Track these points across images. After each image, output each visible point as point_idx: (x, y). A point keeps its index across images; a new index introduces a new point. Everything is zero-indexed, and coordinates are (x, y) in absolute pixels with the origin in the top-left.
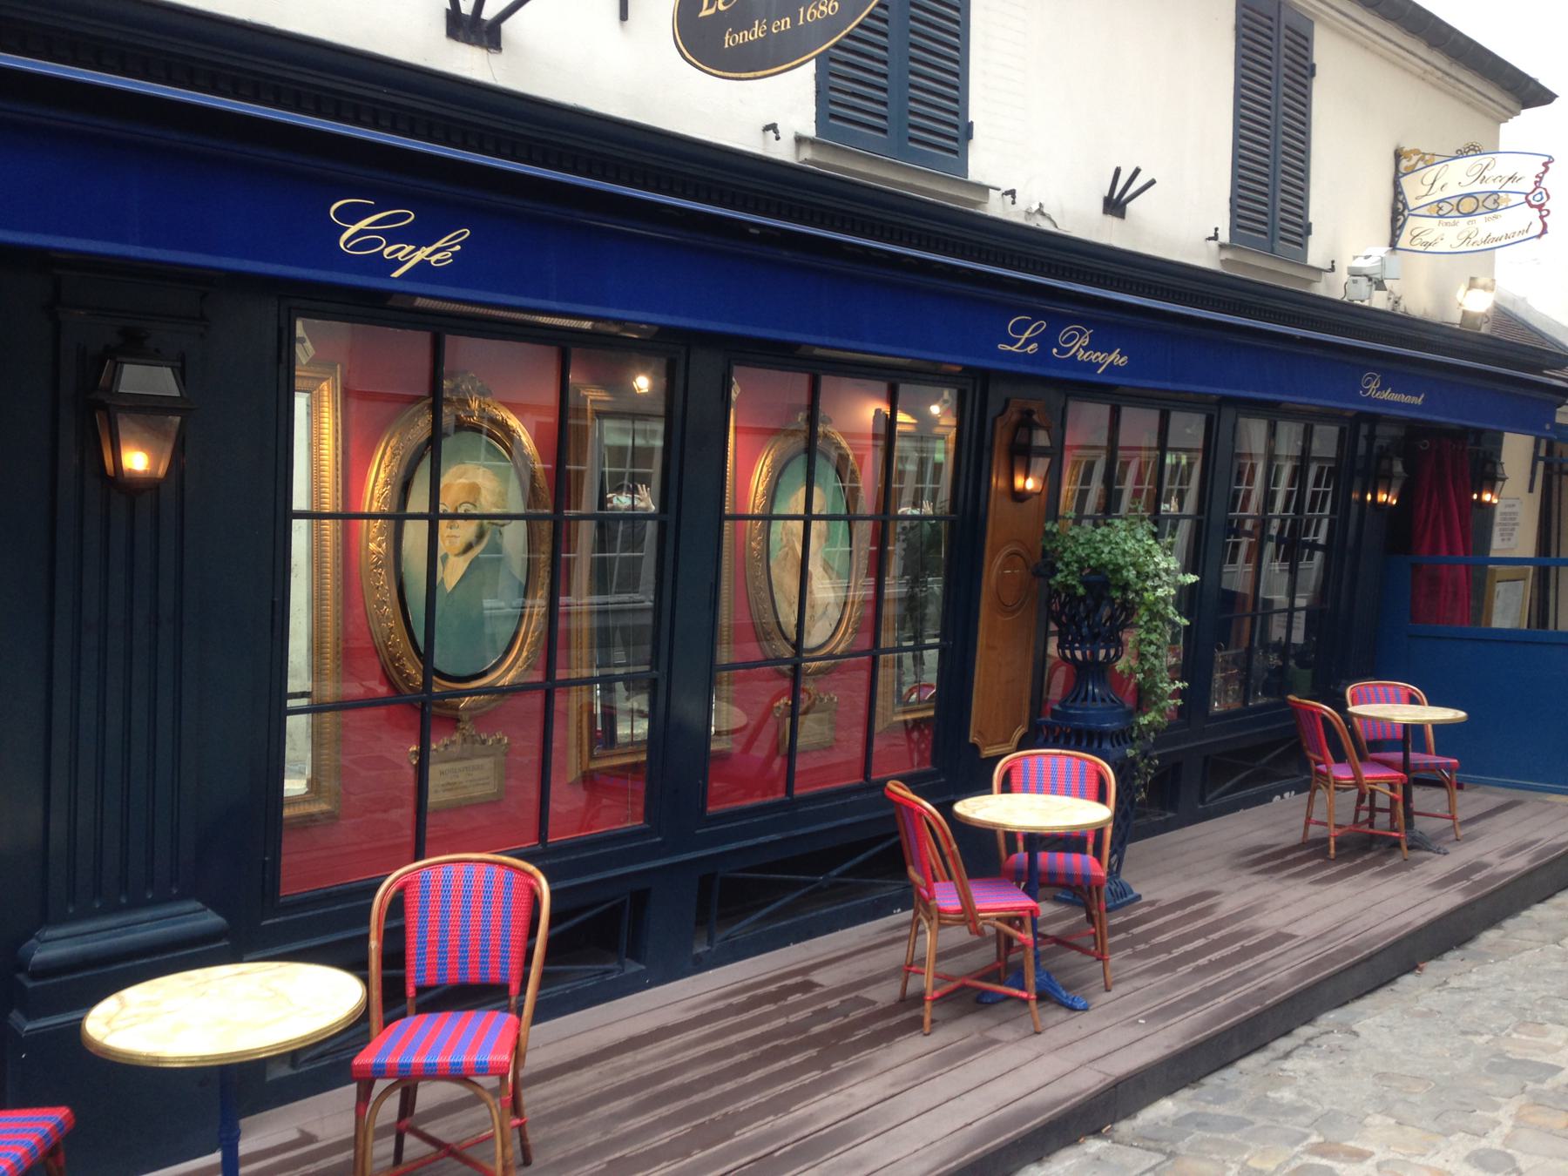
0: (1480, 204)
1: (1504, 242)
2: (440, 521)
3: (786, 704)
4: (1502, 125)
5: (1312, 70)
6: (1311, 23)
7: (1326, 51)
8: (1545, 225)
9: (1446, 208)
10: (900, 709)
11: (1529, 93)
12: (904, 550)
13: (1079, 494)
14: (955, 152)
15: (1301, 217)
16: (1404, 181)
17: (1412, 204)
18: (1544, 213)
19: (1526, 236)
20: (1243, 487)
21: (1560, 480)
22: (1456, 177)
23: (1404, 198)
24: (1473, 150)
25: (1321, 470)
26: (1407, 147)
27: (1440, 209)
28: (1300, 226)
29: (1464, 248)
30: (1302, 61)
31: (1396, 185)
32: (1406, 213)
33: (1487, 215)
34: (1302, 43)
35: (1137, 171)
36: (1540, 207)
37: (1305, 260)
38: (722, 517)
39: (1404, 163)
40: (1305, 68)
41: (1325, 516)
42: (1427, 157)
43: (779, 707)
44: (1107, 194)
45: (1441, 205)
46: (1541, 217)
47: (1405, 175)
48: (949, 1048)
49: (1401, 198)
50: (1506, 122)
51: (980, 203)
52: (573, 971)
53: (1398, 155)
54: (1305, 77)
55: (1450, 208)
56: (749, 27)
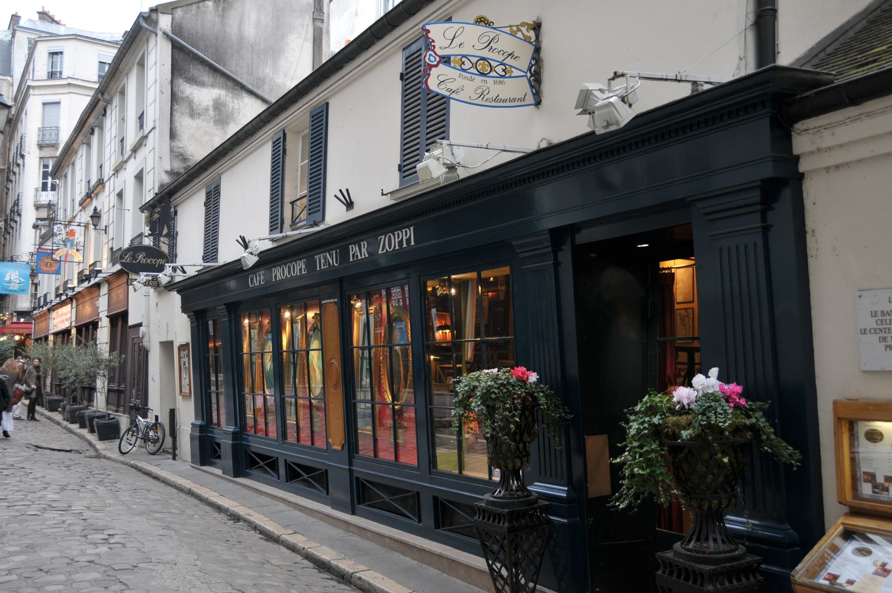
0: (493, 69)
1: (508, 104)
2: (476, 273)
9: (467, 65)
12: (537, 379)
13: (49, 404)
19: (523, 103)
21: (756, 212)
27: (463, 63)
29: (479, 101)
33: (495, 79)
35: (340, 191)
56: (616, 459)
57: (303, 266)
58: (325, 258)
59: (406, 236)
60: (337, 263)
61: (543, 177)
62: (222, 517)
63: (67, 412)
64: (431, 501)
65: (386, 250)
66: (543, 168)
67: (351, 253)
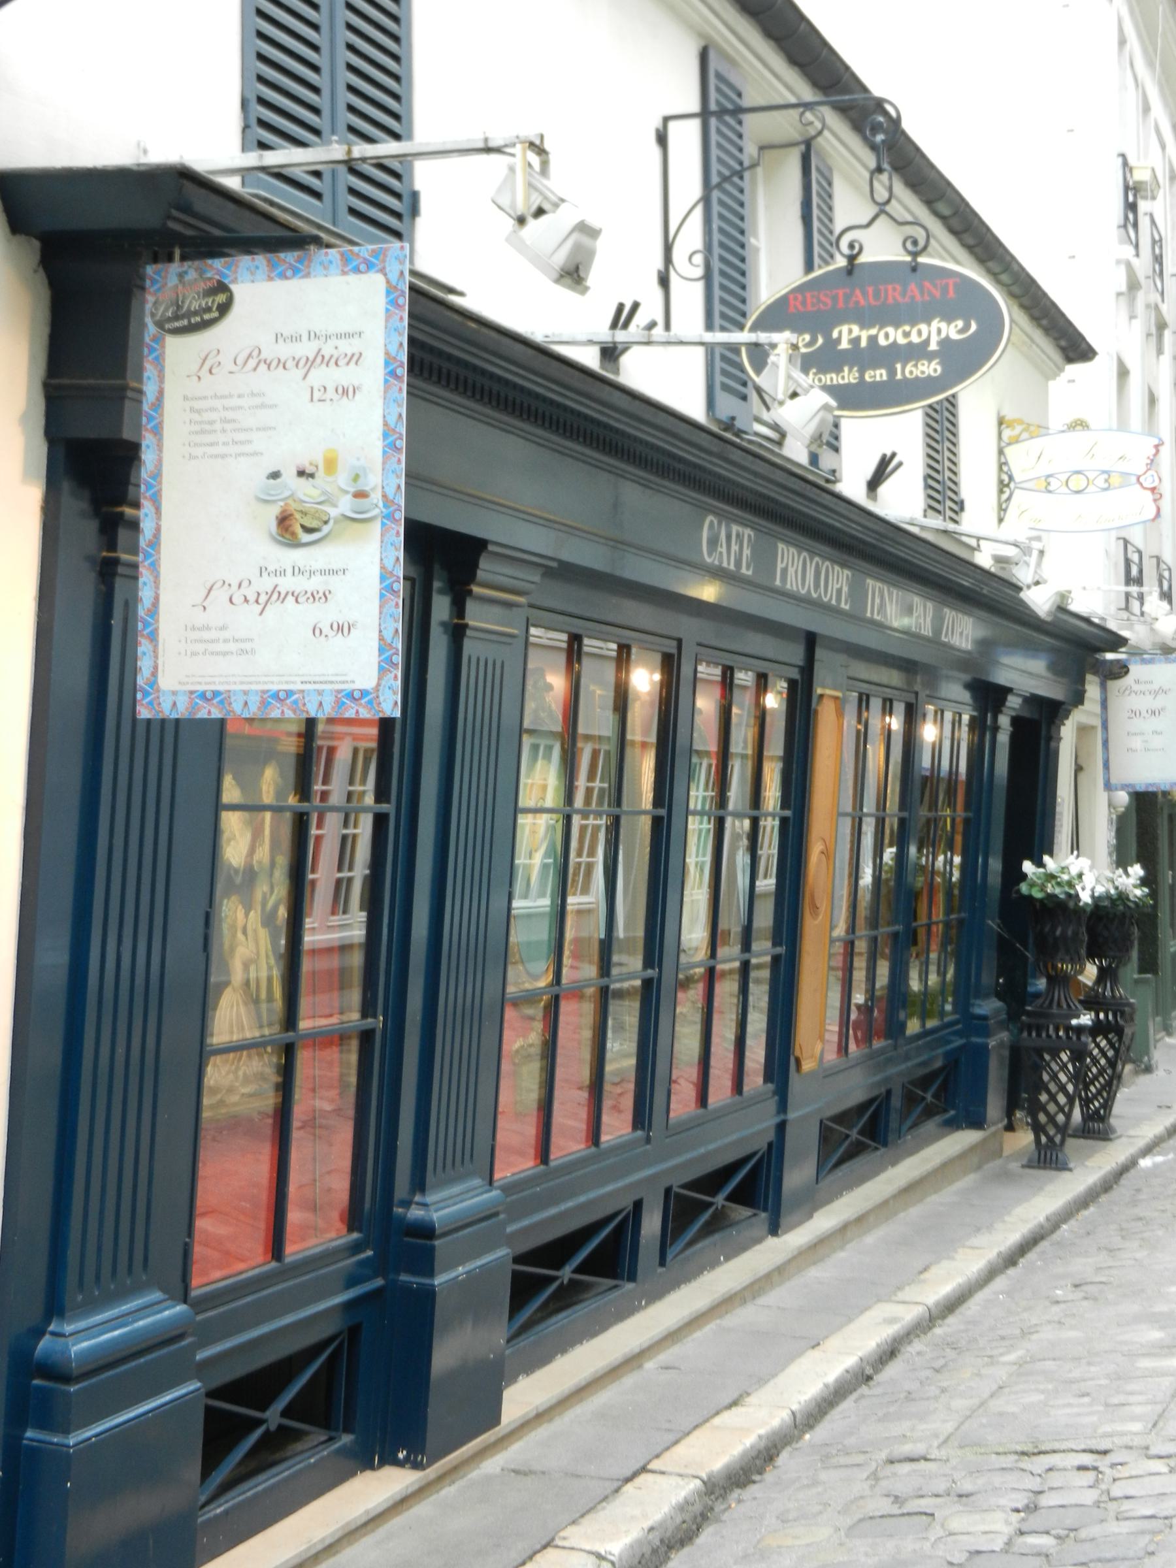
4: (1051, 383)
16: (1008, 451)
17: (1018, 477)
23: (1009, 470)
24: (1081, 425)
25: (595, 754)
31: (1001, 452)
32: (1012, 485)
36: (1153, 490)
39: (1007, 434)
40: (397, 195)
42: (1032, 428)
43: (517, 1051)
45: (1106, 485)
46: (1155, 500)
47: (1009, 444)
48: (103, 1436)
49: (1005, 468)
50: (1055, 379)
53: (1001, 422)
54: (398, 216)
67: (780, 566)
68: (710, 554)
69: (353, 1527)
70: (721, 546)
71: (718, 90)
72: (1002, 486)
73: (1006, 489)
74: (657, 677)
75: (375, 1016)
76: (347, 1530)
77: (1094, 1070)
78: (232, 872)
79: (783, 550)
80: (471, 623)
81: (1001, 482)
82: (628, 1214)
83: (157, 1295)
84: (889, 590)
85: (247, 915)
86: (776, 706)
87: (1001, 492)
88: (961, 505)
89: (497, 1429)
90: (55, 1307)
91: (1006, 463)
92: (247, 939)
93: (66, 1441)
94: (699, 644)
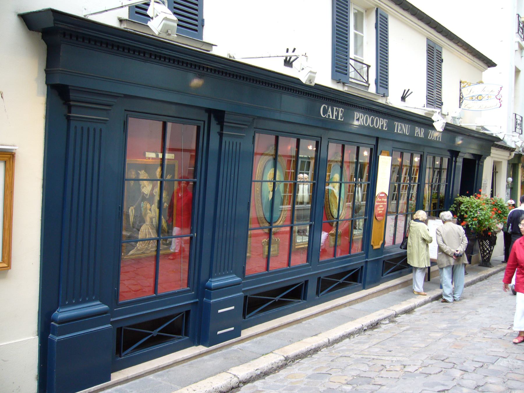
1: (490, 108)
3: (265, 241)
4: (483, 72)
5: (442, 61)
6: (442, 48)
7: (445, 55)
8: (501, 105)
9: (474, 98)
10: (514, 207)
11: (490, 64)
14: (196, 31)
15: (440, 100)
16: (462, 90)
17: (465, 96)
18: (501, 101)
20: (414, 176)
22: (477, 90)
26: (463, 81)
28: (440, 103)
30: (440, 58)
31: (460, 90)
32: (463, 99)
34: (440, 53)
35: (409, 90)
37: (202, 38)
38: (251, 181)
39: (462, 85)
41: (402, 183)
42: (469, 84)
43: (263, 242)
44: (402, 96)
47: (462, 88)
49: (461, 94)
51: (377, 99)
52: (293, 301)
53: (460, 82)
55: (475, 98)
57: (385, 125)
58: (401, 127)
59: (382, 123)
60: (408, 133)
61: (178, 64)
62: (357, 338)
63: (499, 231)
64: (410, 278)
65: (374, 125)
66: (314, 92)
67: (416, 132)
68: (324, 115)
69: (178, 361)
70: (329, 113)
71: (380, 18)
72: (460, 99)
73: (462, 100)
74: (419, 159)
75: (367, 216)
76: (175, 362)
77: (488, 251)
78: (145, 195)
79: (382, 120)
80: (224, 132)
81: (460, 98)
82: (359, 269)
83: (99, 303)
84: (404, 126)
85: (151, 206)
86: (367, 155)
87: (460, 101)
88: (442, 104)
89: (110, 382)
90: (210, 276)
91: (462, 93)
92: (151, 212)
93: (210, 301)
94: (328, 138)
